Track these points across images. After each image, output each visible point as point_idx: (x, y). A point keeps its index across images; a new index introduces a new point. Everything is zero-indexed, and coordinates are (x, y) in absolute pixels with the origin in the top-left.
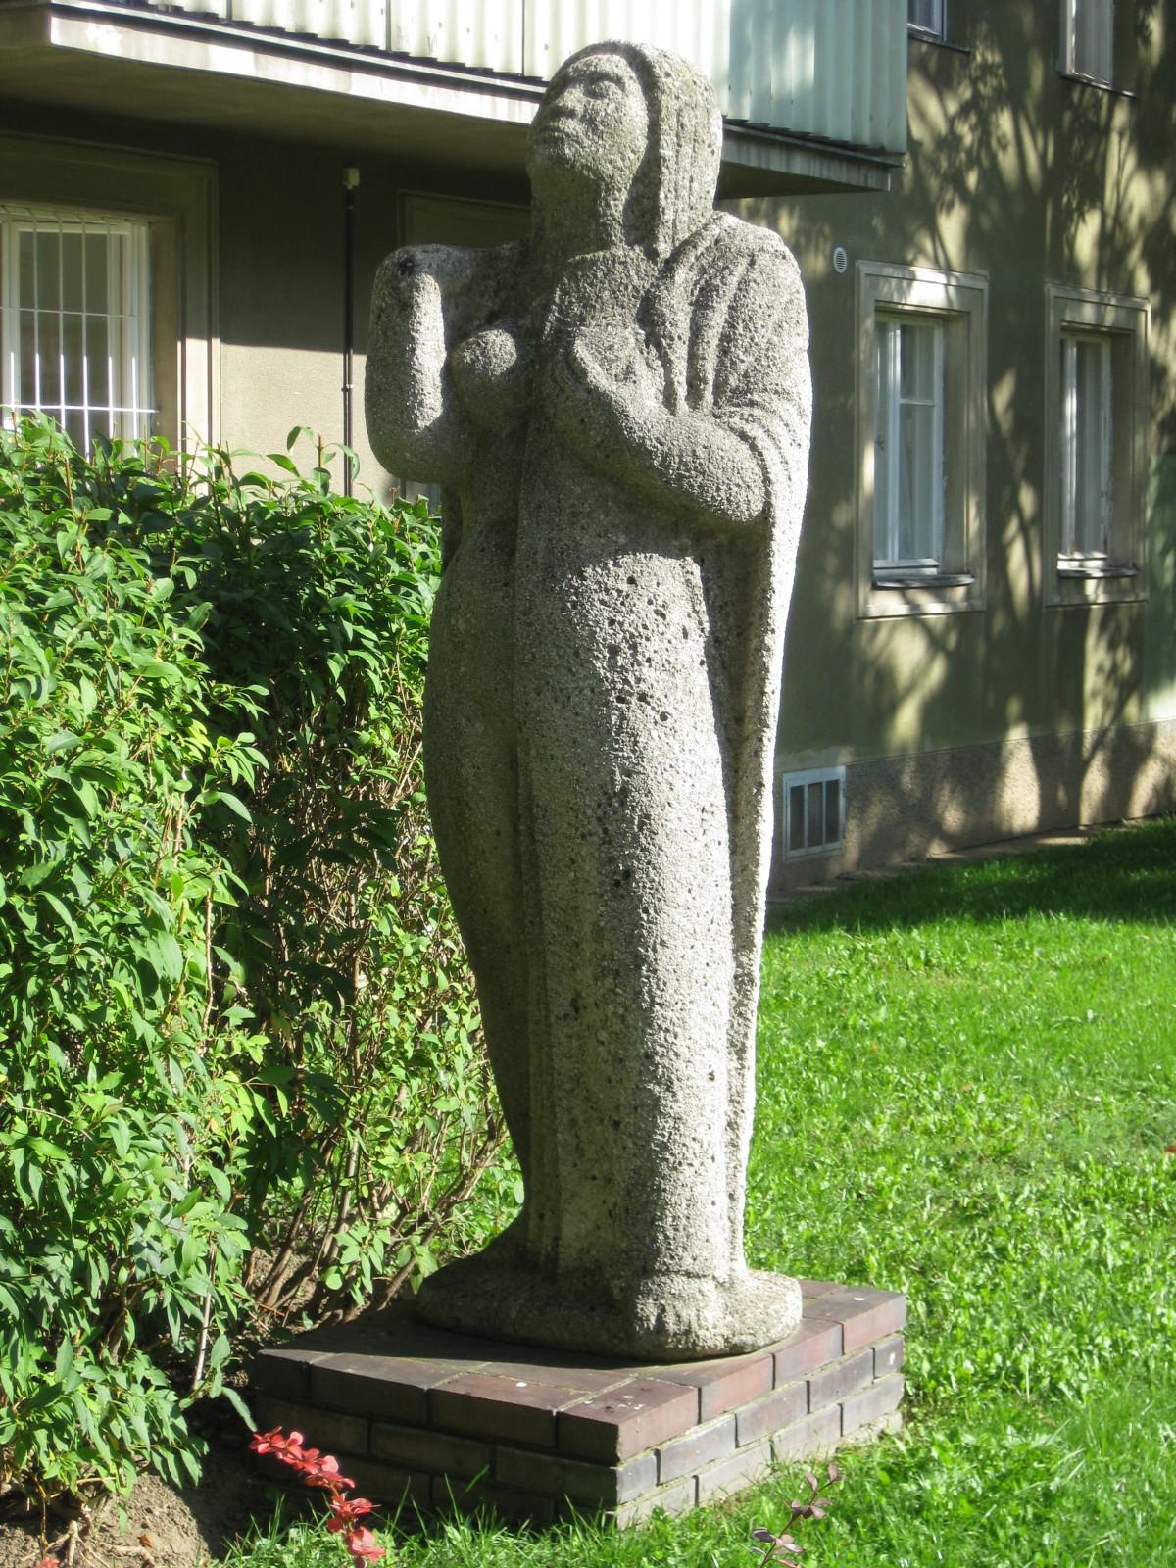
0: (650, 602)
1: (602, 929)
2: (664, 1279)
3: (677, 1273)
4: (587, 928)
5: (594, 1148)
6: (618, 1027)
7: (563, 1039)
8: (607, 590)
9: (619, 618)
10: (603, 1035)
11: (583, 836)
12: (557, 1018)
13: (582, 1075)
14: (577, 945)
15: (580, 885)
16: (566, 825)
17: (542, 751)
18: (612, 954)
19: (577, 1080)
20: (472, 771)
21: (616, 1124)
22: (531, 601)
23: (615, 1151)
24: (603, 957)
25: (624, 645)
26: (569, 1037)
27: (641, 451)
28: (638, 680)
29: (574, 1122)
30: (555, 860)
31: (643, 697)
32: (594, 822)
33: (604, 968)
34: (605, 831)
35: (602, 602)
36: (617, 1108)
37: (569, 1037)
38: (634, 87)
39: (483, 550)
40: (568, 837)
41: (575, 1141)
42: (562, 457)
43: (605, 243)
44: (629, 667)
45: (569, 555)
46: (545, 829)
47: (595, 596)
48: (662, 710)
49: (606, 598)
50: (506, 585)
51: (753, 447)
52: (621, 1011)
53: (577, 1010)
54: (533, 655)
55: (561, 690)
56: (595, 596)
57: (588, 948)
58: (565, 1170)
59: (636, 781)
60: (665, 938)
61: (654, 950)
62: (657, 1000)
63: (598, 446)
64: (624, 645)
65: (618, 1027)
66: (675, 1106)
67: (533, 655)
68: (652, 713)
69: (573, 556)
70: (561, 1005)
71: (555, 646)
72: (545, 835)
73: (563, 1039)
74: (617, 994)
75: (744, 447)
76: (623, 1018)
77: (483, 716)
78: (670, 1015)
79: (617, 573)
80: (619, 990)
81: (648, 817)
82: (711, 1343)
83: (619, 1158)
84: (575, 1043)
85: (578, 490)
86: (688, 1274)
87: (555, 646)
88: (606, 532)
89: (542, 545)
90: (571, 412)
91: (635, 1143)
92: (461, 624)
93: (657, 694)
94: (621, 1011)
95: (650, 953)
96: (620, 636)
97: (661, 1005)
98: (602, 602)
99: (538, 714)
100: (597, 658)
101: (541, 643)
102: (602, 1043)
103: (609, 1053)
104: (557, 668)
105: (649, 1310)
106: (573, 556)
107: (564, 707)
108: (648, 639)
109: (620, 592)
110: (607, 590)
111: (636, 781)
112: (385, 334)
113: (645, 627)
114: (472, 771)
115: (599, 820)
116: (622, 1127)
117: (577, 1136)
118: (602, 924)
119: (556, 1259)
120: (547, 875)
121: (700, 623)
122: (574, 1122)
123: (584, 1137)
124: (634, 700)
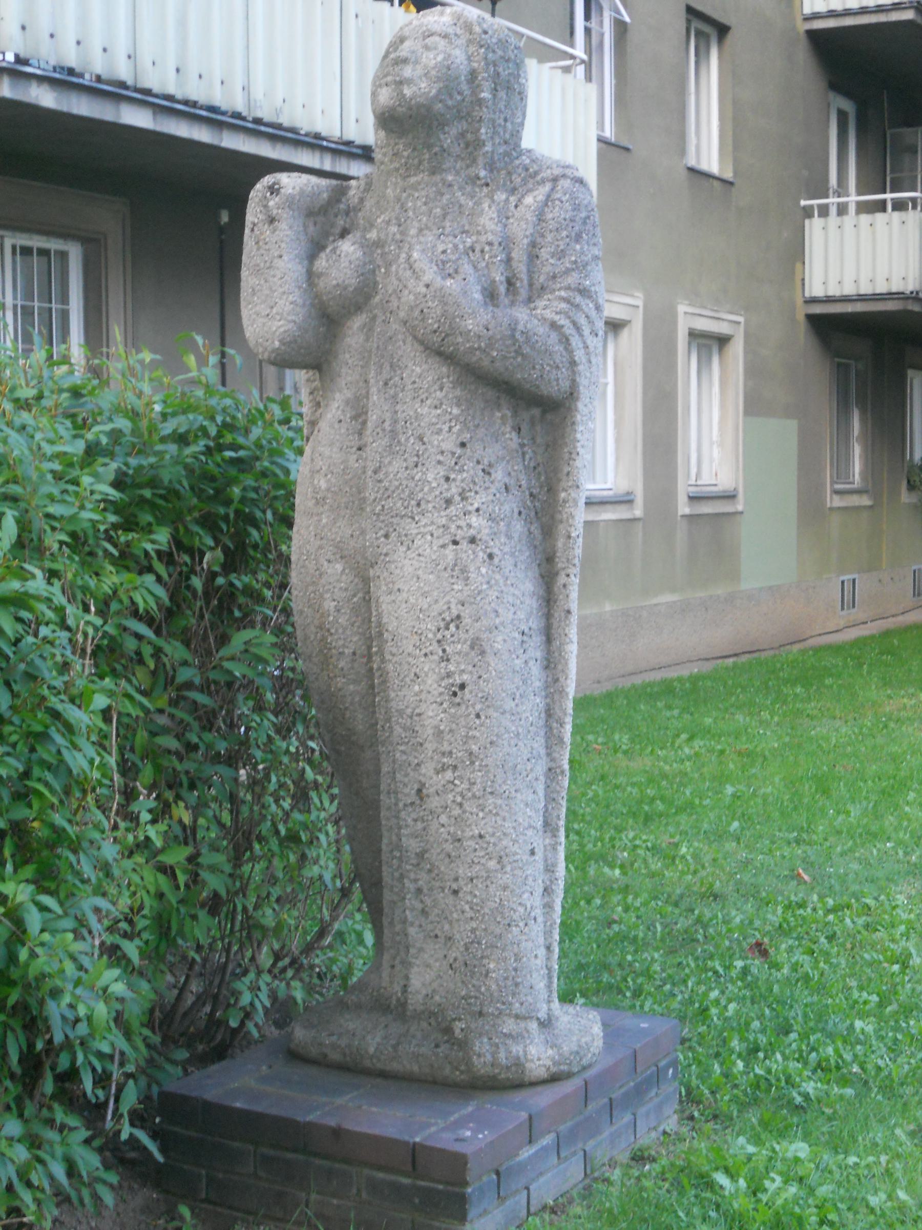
1: (442, 732)
4: (430, 731)
6: (457, 812)
14: (421, 745)
19: (421, 855)
46: (394, 650)
52: (459, 799)
65: (457, 812)
72: (394, 655)
85: (418, 370)
91: (471, 908)
94: (459, 799)
99: (386, 555)
103: (449, 833)
107: (409, 549)
110: (442, 452)
116: (461, 895)
117: (422, 901)
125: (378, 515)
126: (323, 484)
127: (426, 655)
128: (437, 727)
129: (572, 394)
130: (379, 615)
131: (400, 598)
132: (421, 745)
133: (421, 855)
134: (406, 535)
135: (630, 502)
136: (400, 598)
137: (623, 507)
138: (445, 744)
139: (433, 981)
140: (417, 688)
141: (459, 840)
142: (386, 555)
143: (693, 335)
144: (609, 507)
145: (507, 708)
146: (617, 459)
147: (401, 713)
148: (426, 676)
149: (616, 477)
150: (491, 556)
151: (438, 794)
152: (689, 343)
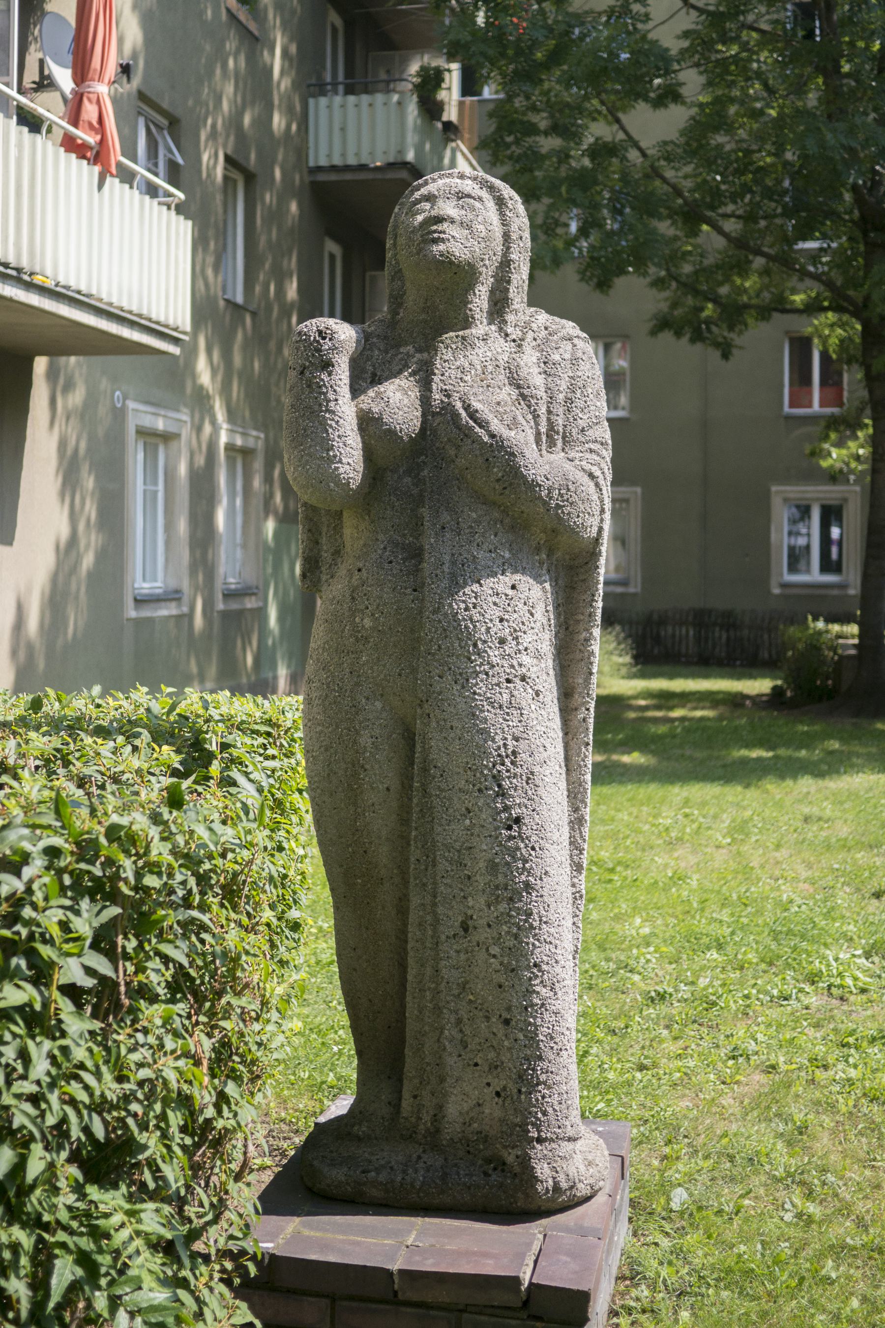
0: (525, 604)
1: (497, 865)
2: (553, 1145)
3: (562, 1139)
4: (482, 864)
5: (477, 1040)
6: (511, 943)
7: (452, 953)
8: (498, 594)
9: (506, 617)
10: (495, 950)
11: (480, 790)
12: (448, 937)
13: (467, 982)
14: (469, 877)
15: (476, 831)
16: (463, 782)
17: (442, 723)
18: (506, 885)
19: (463, 986)
20: (370, 740)
21: (507, 1022)
22: (439, 603)
23: (506, 1043)
24: (497, 887)
25: (510, 638)
26: (458, 952)
27: (532, 486)
28: (520, 665)
29: (459, 1021)
30: (451, 811)
31: (523, 679)
32: (490, 779)
33: (498, 896)
34: (499, 786)
35: (495, 604)
36: (509, 1009)
37: (458, 952)
38: (491, 204)
39: (391, 562)
40: (466, 792)
41: (459, 1036)
42: (459, 488)
43: (467, 323)
44: (513, 655)
45: (469, 566)
46: (443, 786)
47: (489, 599)
48: (536, 688)
49: (497, 601)
50: (415, 590)
51: (597, 485)
52: (515, 930)
53: (466, 930)
54: (439, 646)
55: (461, 674)
56: (489, 599)
57: (481, 881)
58: (451, 1060)
59: (522, 745)
60: (548, 869)
61: (541, 879)
62: (544, 919)
63: (498, 480)
64: (510, 638)
65: (511, 943)
66: (556, 1003)
67: (439, 646)
68: (530, 691)
69: (472, 567)
70: (451, 924)
71: (459, 639)
72: (442, 791)
73: (452, 953)
74: (511, 916)
75: (592, 484)
76: (516, 936)
77: (382, 695)
78: (552, 930)
79: (503, 582)
80: (513, 913)
81: (532, 773)
82: (584, 1192)
83: (509, 1049)
84: (463, 956)
85: (474, 515)
86: (570, 1139)
87: (459, 639)
88: (496, 548)
89: (447, 558)
90: (478, 452)
91: (525, 1036)
92: (368, 623)
93: (533, 676)
94: (515, 930)
95: (539, 882)
96: (507, 631)
97: (545, 923)
98: (495, 604)
99: (440, 693)
100: (490, 648)
101: (446, 637)
102: (494, 956)
103: (501, 964)
104: (458, 657)
105: (542, 1170)
106: (472, 567)
107: (463, 687)
108: (525, 633)
109: (506, 595)
110: (498, 594)
111: (522, 745)
112: (309, 386)
113: (523, 623)
114: (370, 740)
115: (494, 777)
116: (513, 1023)
117: (461, 1031)
118: (497, 860)
119: (438, 1131)
120: (444, 822)
121: (549, 620)
122: (459, 1021)
123: (468, 1032)
124: (517, 680)
125: (434, 655)
126: (368, 623)
127: (480, 790)
128: (491, 861)
129: (597, 540)
130: (426, 751)
131: (452, 735)
132: (469, 877)
133: (463, 986)
134: (461, 674)
135: (178, 600)
136: (452, 735)
137: (173, 604)
138: (500, 876)
139: (471, 1109)
140: (467, 822)
141: (513, 970)
142: (440, 693)
143: (142, 432)
144: (163, 604)
145: (555, 839)
146: (167, 560)
147: (448, 847)
148: (481, 811)
149: (165, 576)
150: (537, 693)
151: (489, 926)
152: (136, 441)
